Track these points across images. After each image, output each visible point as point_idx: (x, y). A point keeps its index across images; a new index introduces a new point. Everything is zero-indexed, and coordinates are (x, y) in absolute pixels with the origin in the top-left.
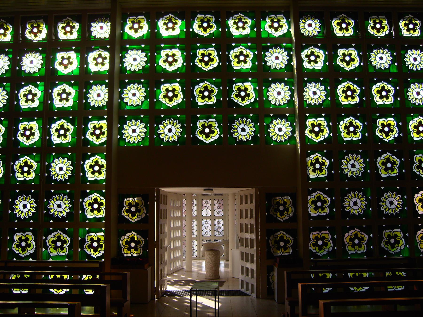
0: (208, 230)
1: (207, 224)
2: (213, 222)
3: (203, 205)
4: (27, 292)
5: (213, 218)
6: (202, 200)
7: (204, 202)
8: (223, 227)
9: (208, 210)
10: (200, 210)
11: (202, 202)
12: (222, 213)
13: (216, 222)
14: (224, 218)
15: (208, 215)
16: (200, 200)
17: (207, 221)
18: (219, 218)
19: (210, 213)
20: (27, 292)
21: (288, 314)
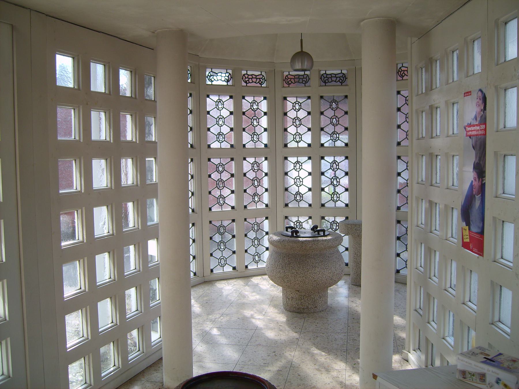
0: (303, 190)
1: (300, 175)
2: (317, 166)
3: (285, 114)
4: (129, 138)
5: (316, 152)
6: (285, 98)
7: (289, 106)
8: (345, 197)
9: (302, 130)
10: (278, 129)
11: (284, 106)
12: (345, 138)
13: (325, 165)
14: (350, 151)
15: (302, 145)
16: (280, 159)
17: (298, 162)
18: (334, 151)
19: (308, 138)
20: (130, 161)
21: (485, 358)
